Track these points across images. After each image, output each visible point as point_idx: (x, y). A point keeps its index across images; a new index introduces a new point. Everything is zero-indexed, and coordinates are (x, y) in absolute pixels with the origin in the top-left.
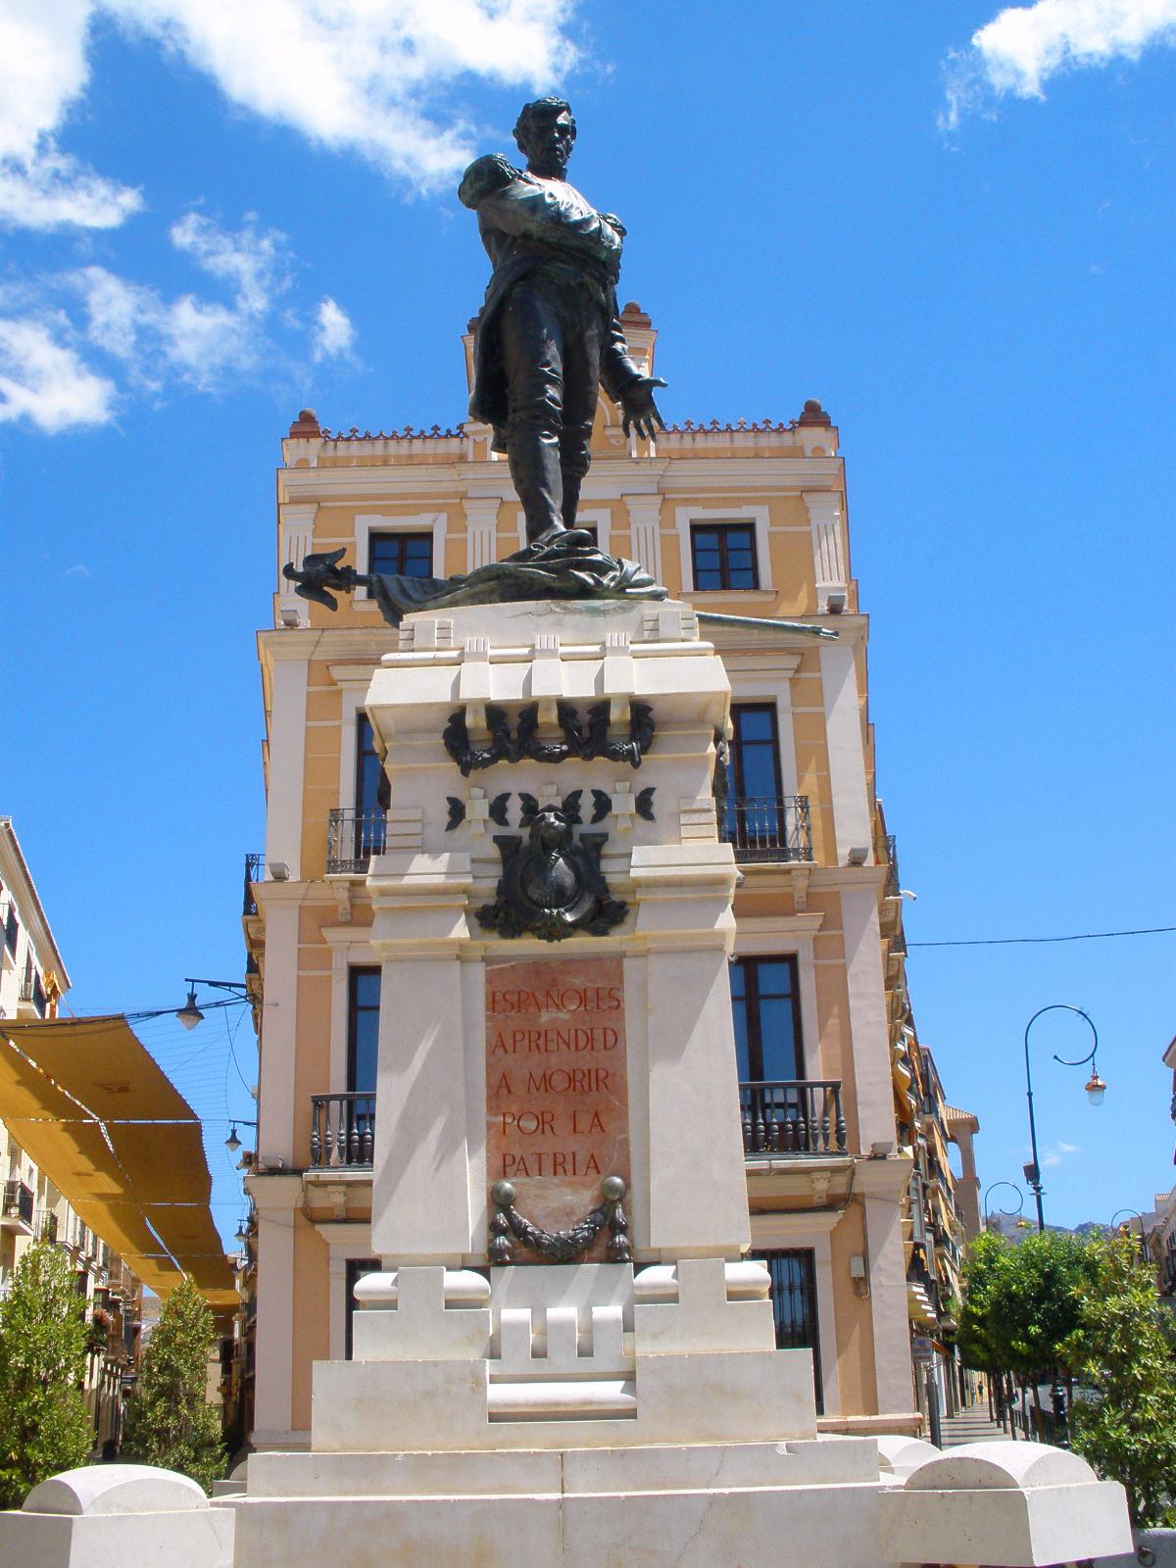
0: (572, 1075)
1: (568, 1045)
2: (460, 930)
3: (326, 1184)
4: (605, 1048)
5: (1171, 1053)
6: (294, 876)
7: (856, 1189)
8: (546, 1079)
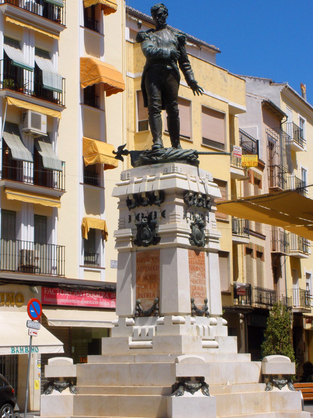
2: (130, 245)
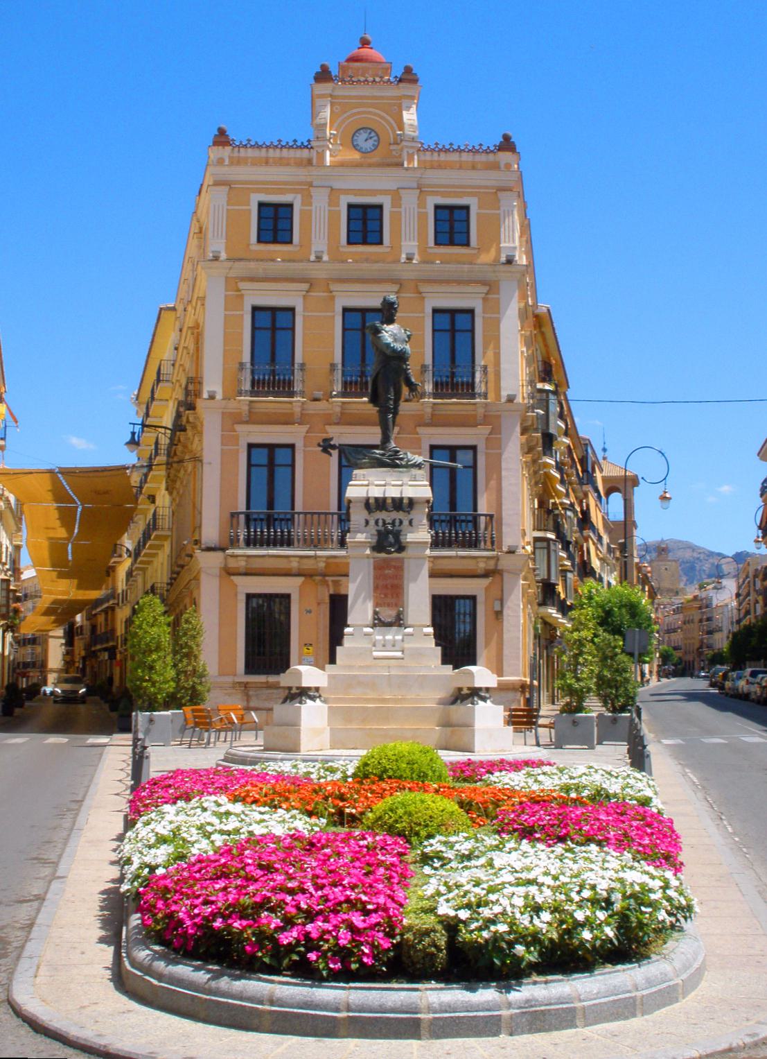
2: (368, 552)
3: (237, 556)
5: (764, 449)
6: (219, 396)
7: (499, 568)
8: (386, 586)
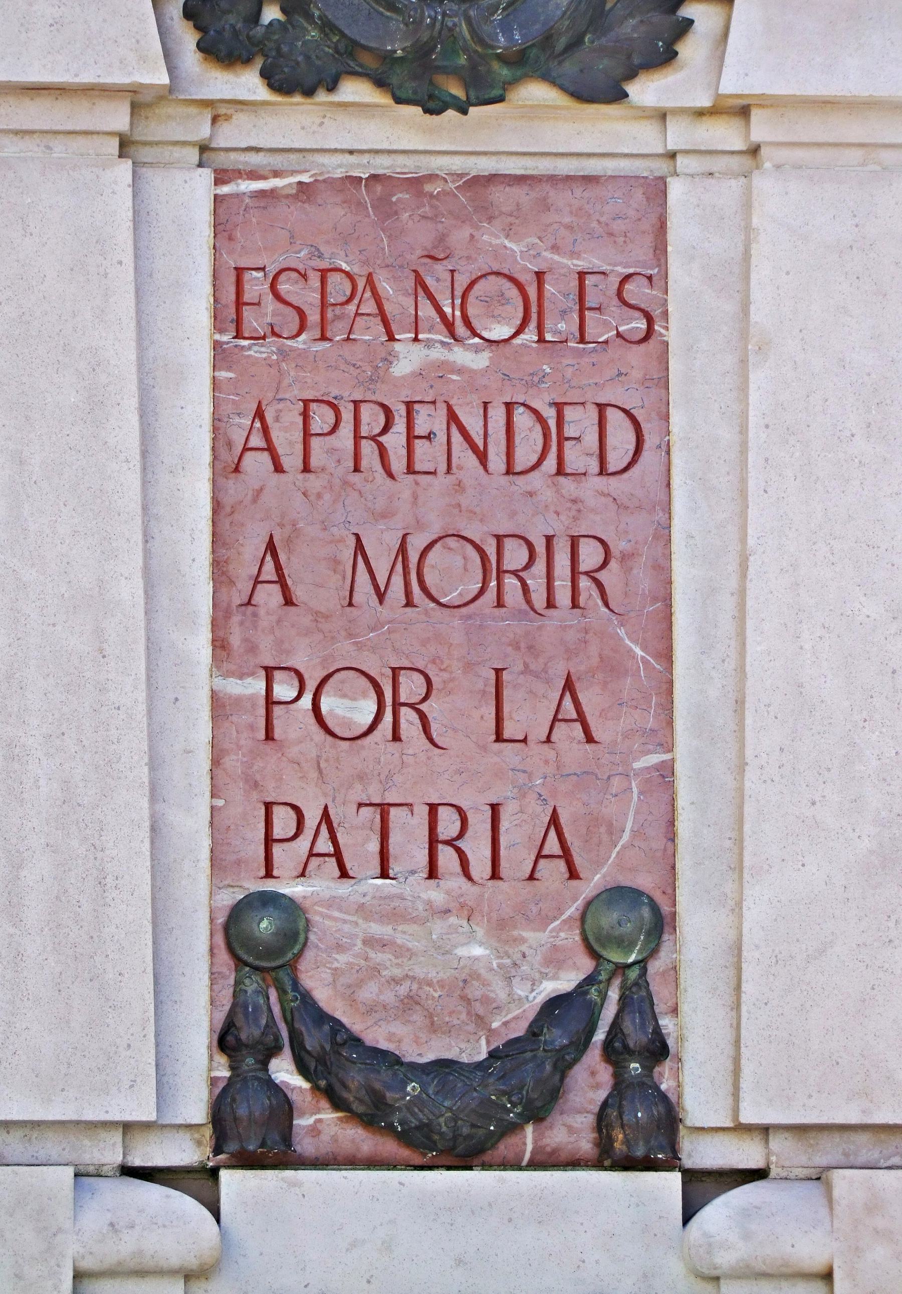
0: (491, 551)
1: (482, 457)
4: (603, 471)
